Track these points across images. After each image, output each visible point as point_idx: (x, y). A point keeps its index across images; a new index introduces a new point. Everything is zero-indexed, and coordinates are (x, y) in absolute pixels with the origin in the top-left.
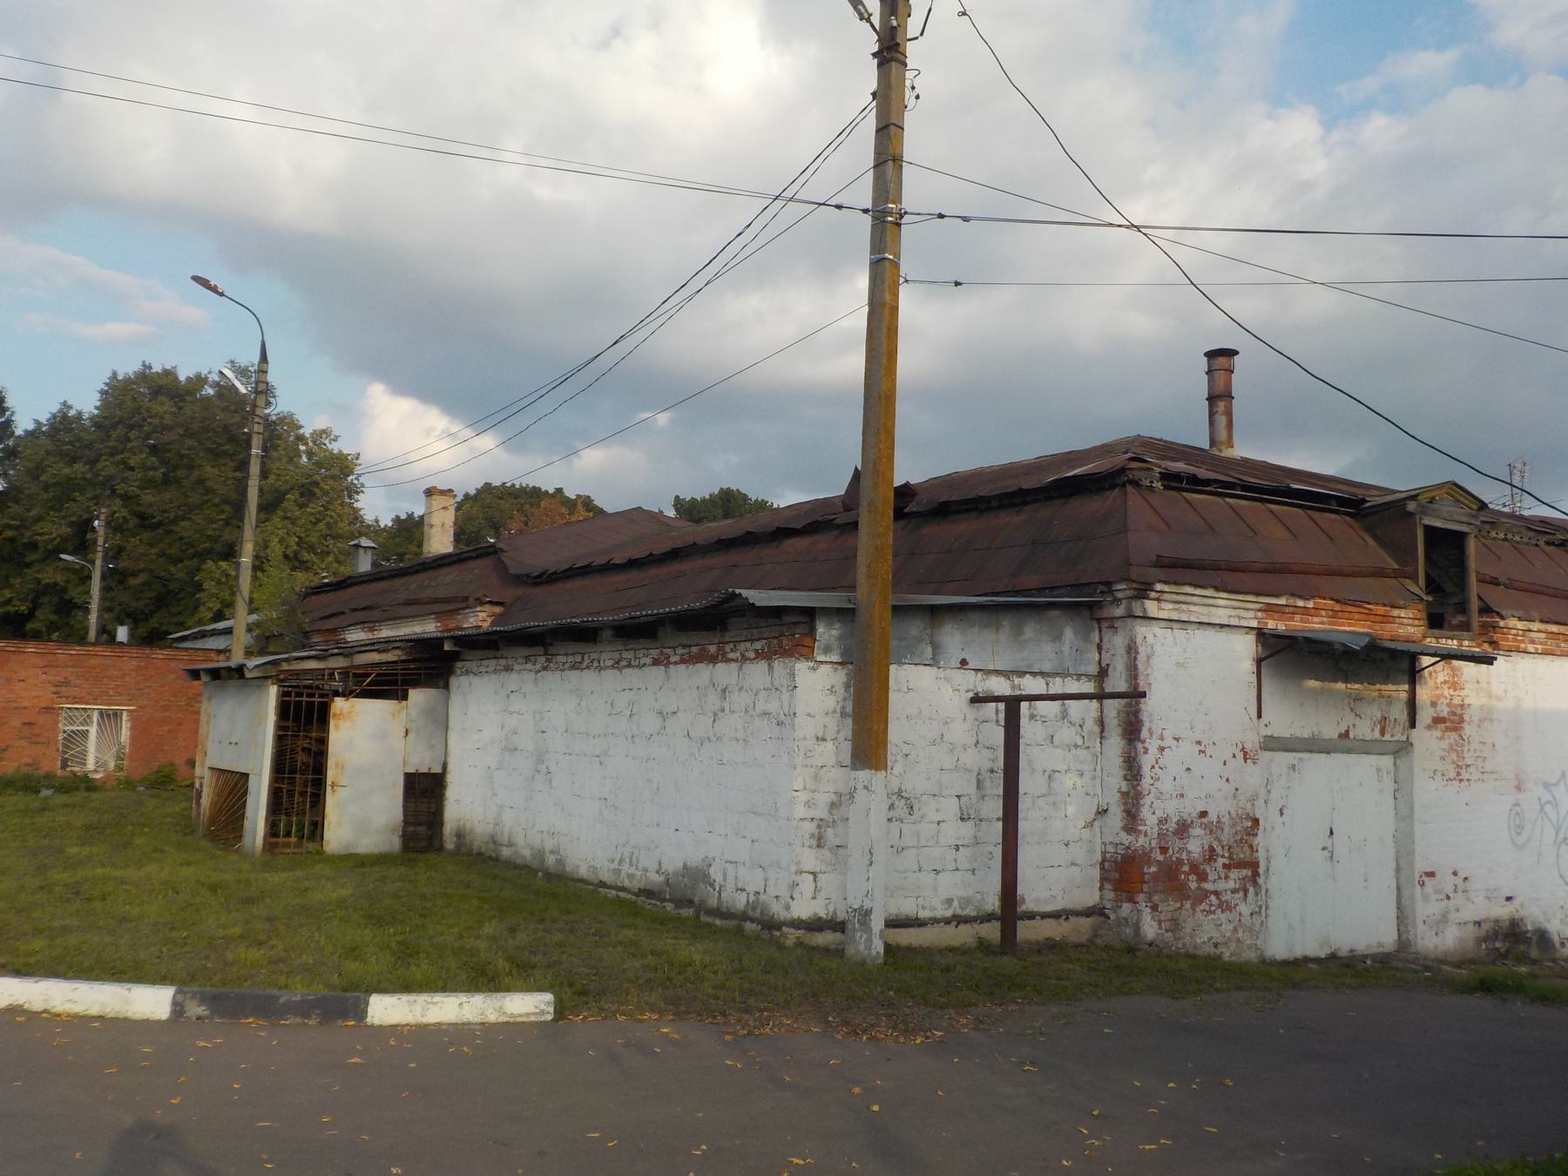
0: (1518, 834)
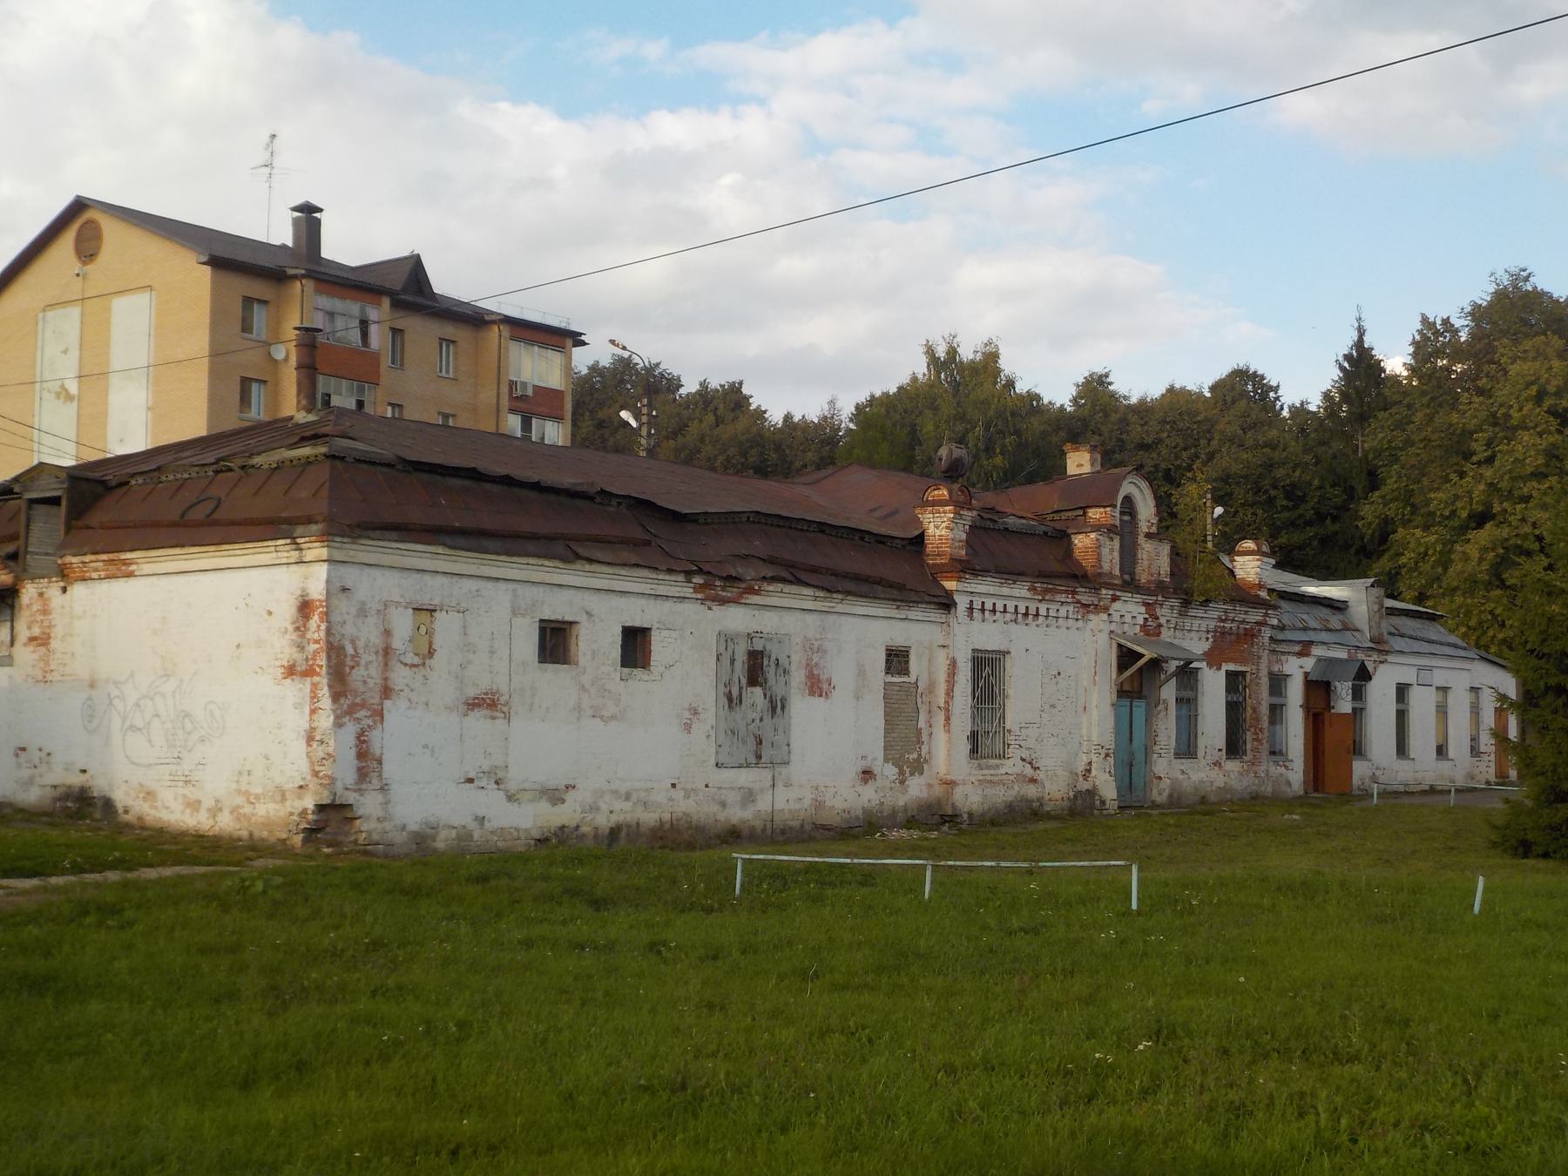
0: (89, 721)
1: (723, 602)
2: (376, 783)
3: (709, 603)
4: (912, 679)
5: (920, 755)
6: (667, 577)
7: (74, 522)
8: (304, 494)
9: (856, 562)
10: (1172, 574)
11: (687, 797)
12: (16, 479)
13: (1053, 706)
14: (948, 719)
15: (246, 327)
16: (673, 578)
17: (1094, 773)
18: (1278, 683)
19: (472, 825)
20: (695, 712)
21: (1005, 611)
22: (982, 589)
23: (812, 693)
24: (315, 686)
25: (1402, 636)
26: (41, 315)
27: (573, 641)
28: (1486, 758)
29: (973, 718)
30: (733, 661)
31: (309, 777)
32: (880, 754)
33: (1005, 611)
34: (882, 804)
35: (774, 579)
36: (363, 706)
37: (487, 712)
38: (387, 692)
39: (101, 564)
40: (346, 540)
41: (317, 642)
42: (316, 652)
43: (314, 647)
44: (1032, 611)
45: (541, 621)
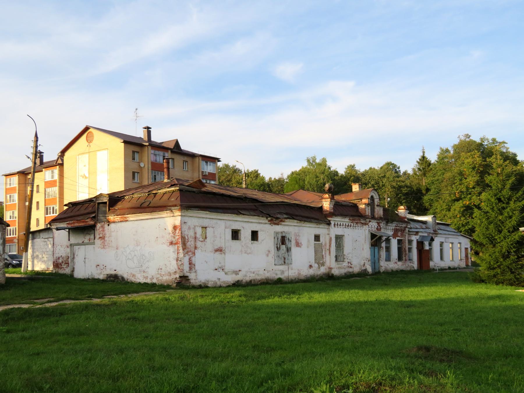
1: (275, 224)
2: (194, 270)
3: (272, 224)
4: (321, 242)
5: (323, 261)
6: (262, 218)
7: (110, 208)
8: (173, 200)
9: (306, 214)
10: (383, 215)
11: (268, 273)
12: (94, 198)
13: (355, 249)
14: (330, 252)
15: (134, 159)
16: (263, 218)
17: (366, 265)
18: (410, 242)
19: (217, 280)
20: (269, 252)
21: (343, 225)
22: (337, 220)
23: (297, 246)
24: (178, 247)
25: (441, 230)
26: (78, 157)
27: (239, 234)
28: (463, 260)
29: (336, 252)
30: (278, 239)
31: (177, 270)
32: (314, 261)
33: (343, 225)
34: (314, 274)
35: (286, 218)
36: (190, 251)
37: (220, 252)
38: (196, 248)
39: (119, 218)
40: (185, 210)
41: (178, 236)
42: (178, 239)
43: (177, 237)
44: (350, 225)
45: (232, 230)
